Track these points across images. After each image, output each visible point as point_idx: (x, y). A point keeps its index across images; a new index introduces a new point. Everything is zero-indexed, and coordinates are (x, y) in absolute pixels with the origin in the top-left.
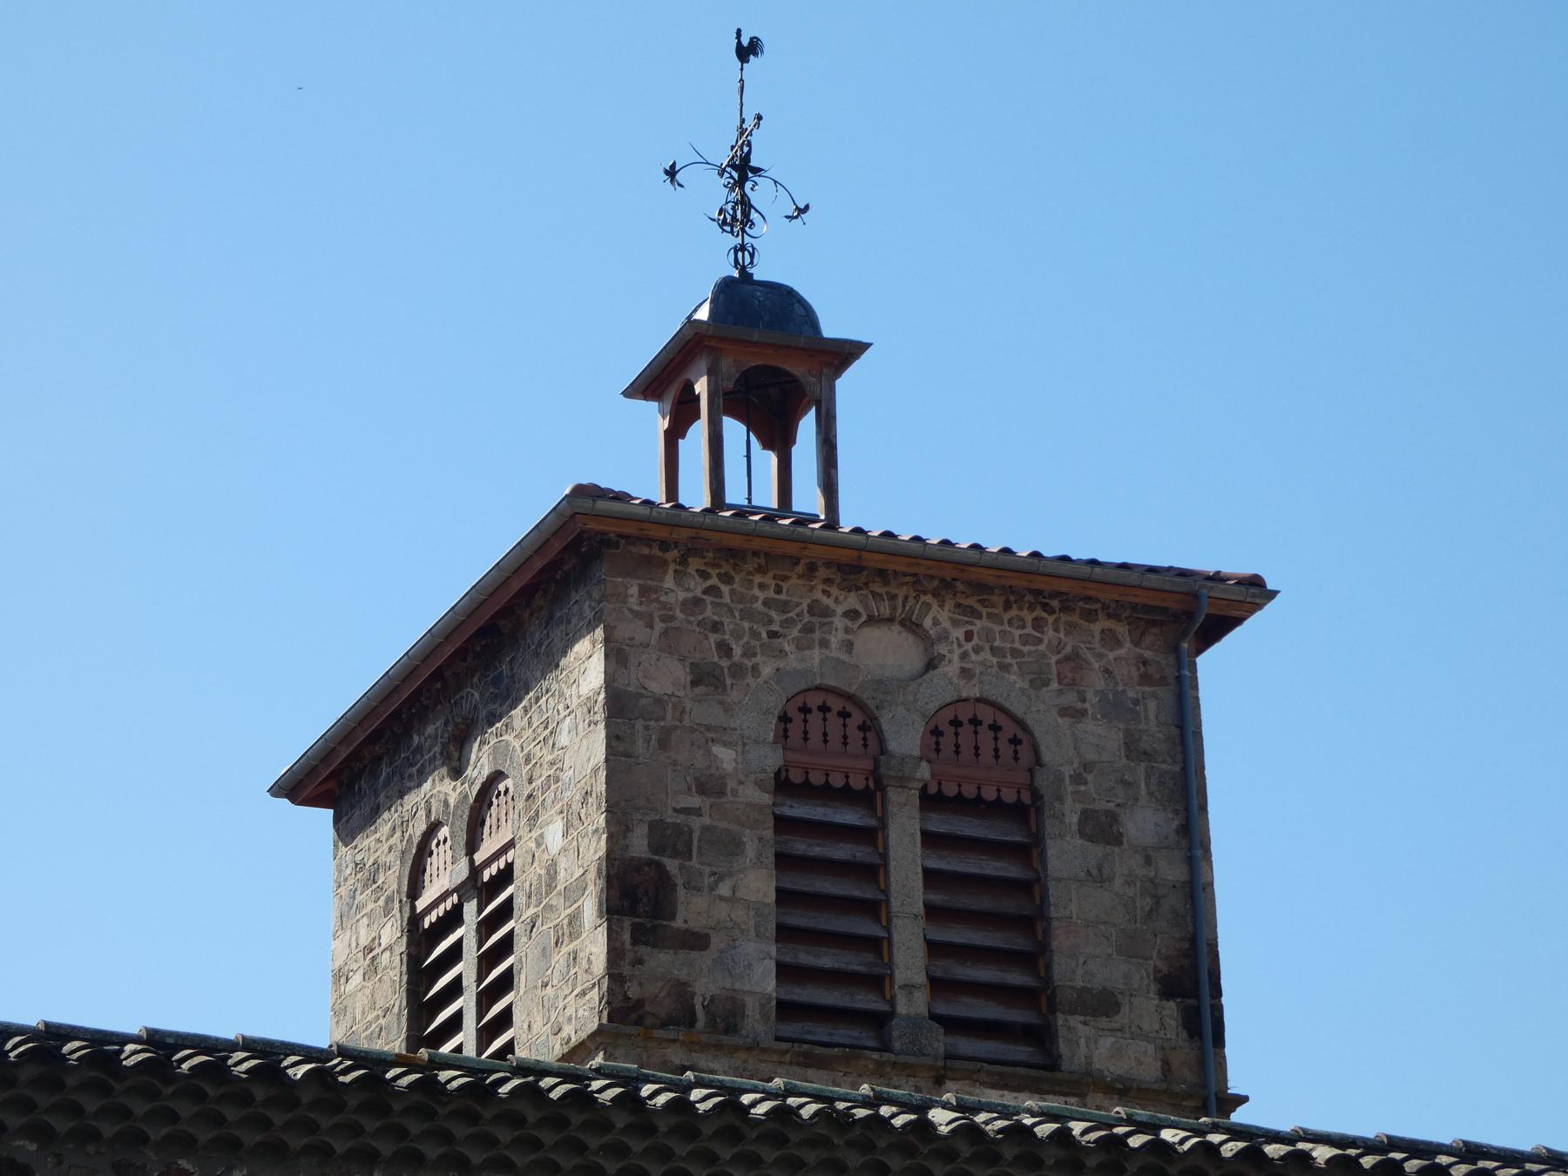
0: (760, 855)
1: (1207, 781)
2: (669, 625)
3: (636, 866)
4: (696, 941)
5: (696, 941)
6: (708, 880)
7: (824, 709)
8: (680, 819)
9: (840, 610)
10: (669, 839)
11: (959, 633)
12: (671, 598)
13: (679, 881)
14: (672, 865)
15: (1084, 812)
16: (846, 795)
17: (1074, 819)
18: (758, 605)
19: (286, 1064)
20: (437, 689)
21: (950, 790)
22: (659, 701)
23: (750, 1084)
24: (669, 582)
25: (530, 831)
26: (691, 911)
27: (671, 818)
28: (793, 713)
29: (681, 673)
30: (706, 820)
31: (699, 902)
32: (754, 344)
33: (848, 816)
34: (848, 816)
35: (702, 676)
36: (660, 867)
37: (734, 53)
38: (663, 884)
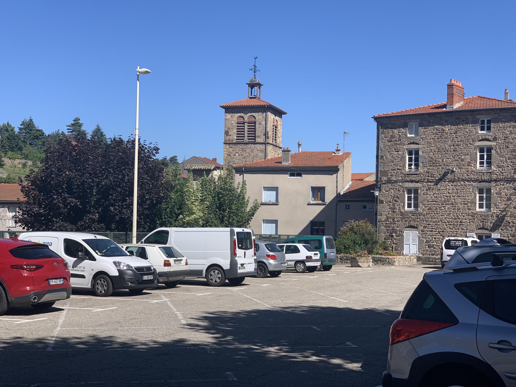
3: (226, 131)
4: (230, 135)
5: (230, 135)
9: (242, 110)
10: (229, 129)
11: (250, 110)
13: (229, 131)
14: (229, 130)
15: (259, 123)
16: (253, 123)
17: (258, 123)
19: (277, 347)
20: (116, 204)
23: (285, 163)
24: (229, 110)
26: (230, 133)
32: (60, 338)
33: (242, 125)
34: (242, 125)
36: (228, 131)
37: (157, 270)
38: (228, 132)
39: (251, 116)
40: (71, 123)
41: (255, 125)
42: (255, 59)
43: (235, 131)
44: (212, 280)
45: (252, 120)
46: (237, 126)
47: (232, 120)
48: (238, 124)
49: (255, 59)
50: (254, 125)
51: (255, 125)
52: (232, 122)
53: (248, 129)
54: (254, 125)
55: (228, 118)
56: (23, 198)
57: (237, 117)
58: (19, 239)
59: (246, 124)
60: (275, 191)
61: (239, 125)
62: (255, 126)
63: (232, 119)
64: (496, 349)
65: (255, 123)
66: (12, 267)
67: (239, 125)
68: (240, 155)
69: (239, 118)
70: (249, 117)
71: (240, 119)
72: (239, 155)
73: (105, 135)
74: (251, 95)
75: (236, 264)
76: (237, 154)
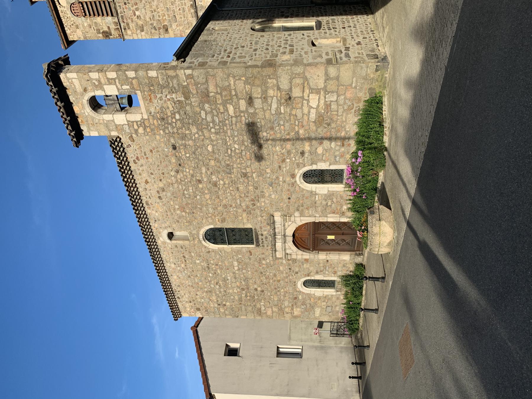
0: (95, 20)
1: (238, 22)
2: (71, 17)
4: (109, 27)
5: (109, 27)
6: (101, 26)
7: (73, 7)
8: (95, 30)
12: (70, 32)
13: (103, 30)
14: (101, 31)
16: (83, 6)
18: (65, 20)
21: (84, 14)
22: (83, 33)
25: (165, 167)
26: (106, 29)
27: (96, 31)
28: (76, 14)
29: (78, 30)
30: (94, 27)
31: (104, 28)
35: (77, 27)
36: (102, 33)
39: (72, 8)
40: (124, 185)
43: (99, 19)
44: (347, 7)
48: (86, 15)
52: (85, 26)
61: (87, 13)
63: (81, 26)
64: (211, 25)
66: (129, 146)
67: (87, 13)
68: (137, 7)
72: (137, 9)
73: (313, 324)
76: (137, 13)
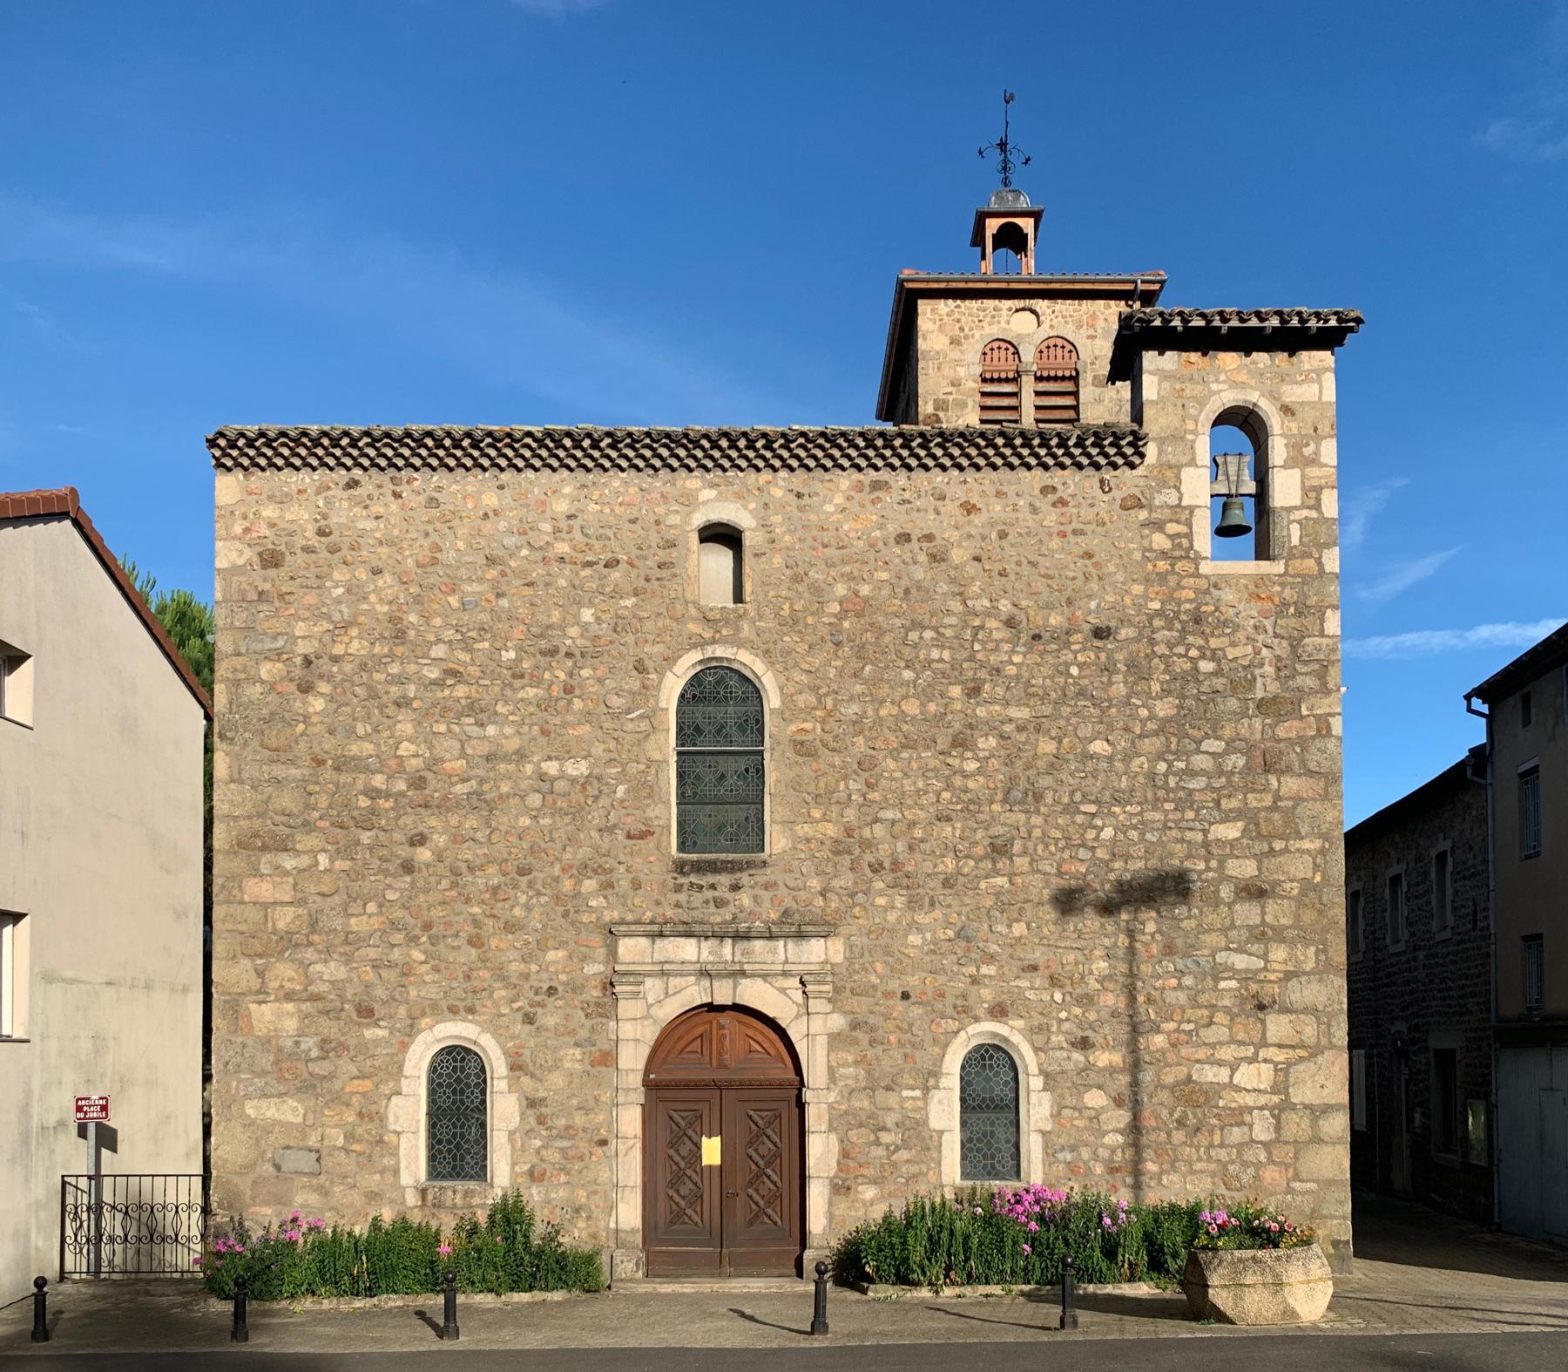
14: (941, 415)
41: (1077, 386)
42: (1007, 102)
45: (1002, 365)
46: (984, 394)
47: (958, 363)
48: (984, 380)
49: (1007, 102)
50: (1068, 386)
51: (1016, 390)
53: (1038, 408)
54: (1068, 386)
55: (937, 348)
56: (668, 673)
57: (980, 347)
58: (1324, 443)
59: (1028, 386)
60: (1339, 514)
62: (1075, 394)
63: (954, 354)
65: (1075, 379)
69: (989, 352)
70: (996, 345)
71: (1052, 357)
74: (1143, 282)
75: (1161, 1249)
